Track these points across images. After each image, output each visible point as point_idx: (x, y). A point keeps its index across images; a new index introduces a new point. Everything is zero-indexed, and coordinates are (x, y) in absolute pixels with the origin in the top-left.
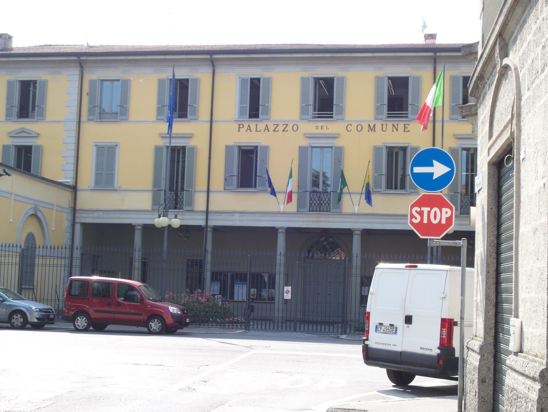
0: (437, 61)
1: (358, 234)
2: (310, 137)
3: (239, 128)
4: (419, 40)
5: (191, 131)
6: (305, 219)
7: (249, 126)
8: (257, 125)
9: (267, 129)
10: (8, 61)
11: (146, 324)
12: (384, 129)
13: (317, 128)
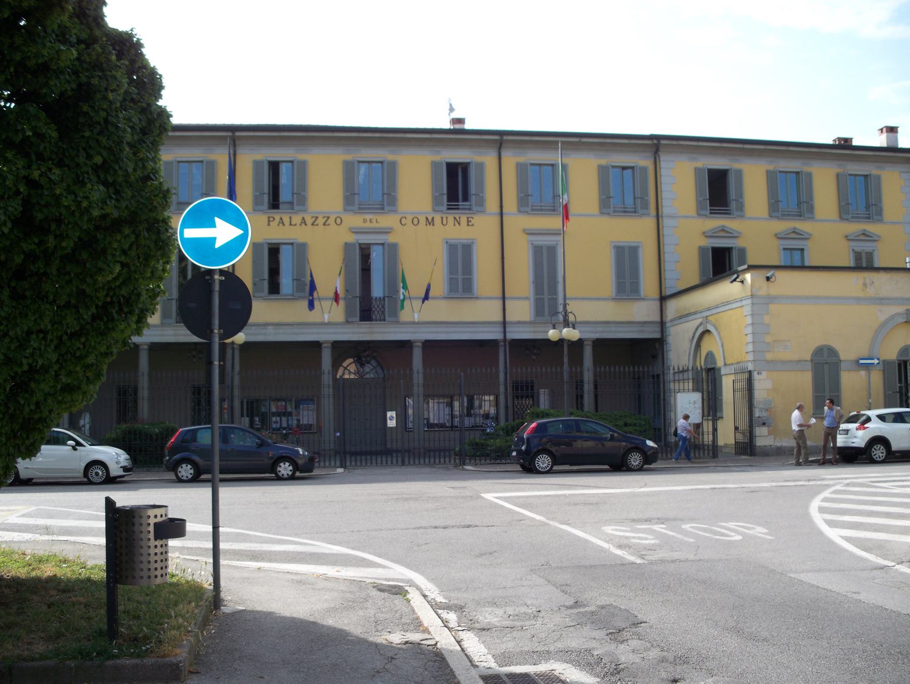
0: (237, 142)
2: (355, 231)
4: (445, 124)
5: (350, 227)
6: (356, 330)
9: (304, 222)
10: (698, 146)
11: (273, 468)
12: (444, 223)
13: (365, 221)
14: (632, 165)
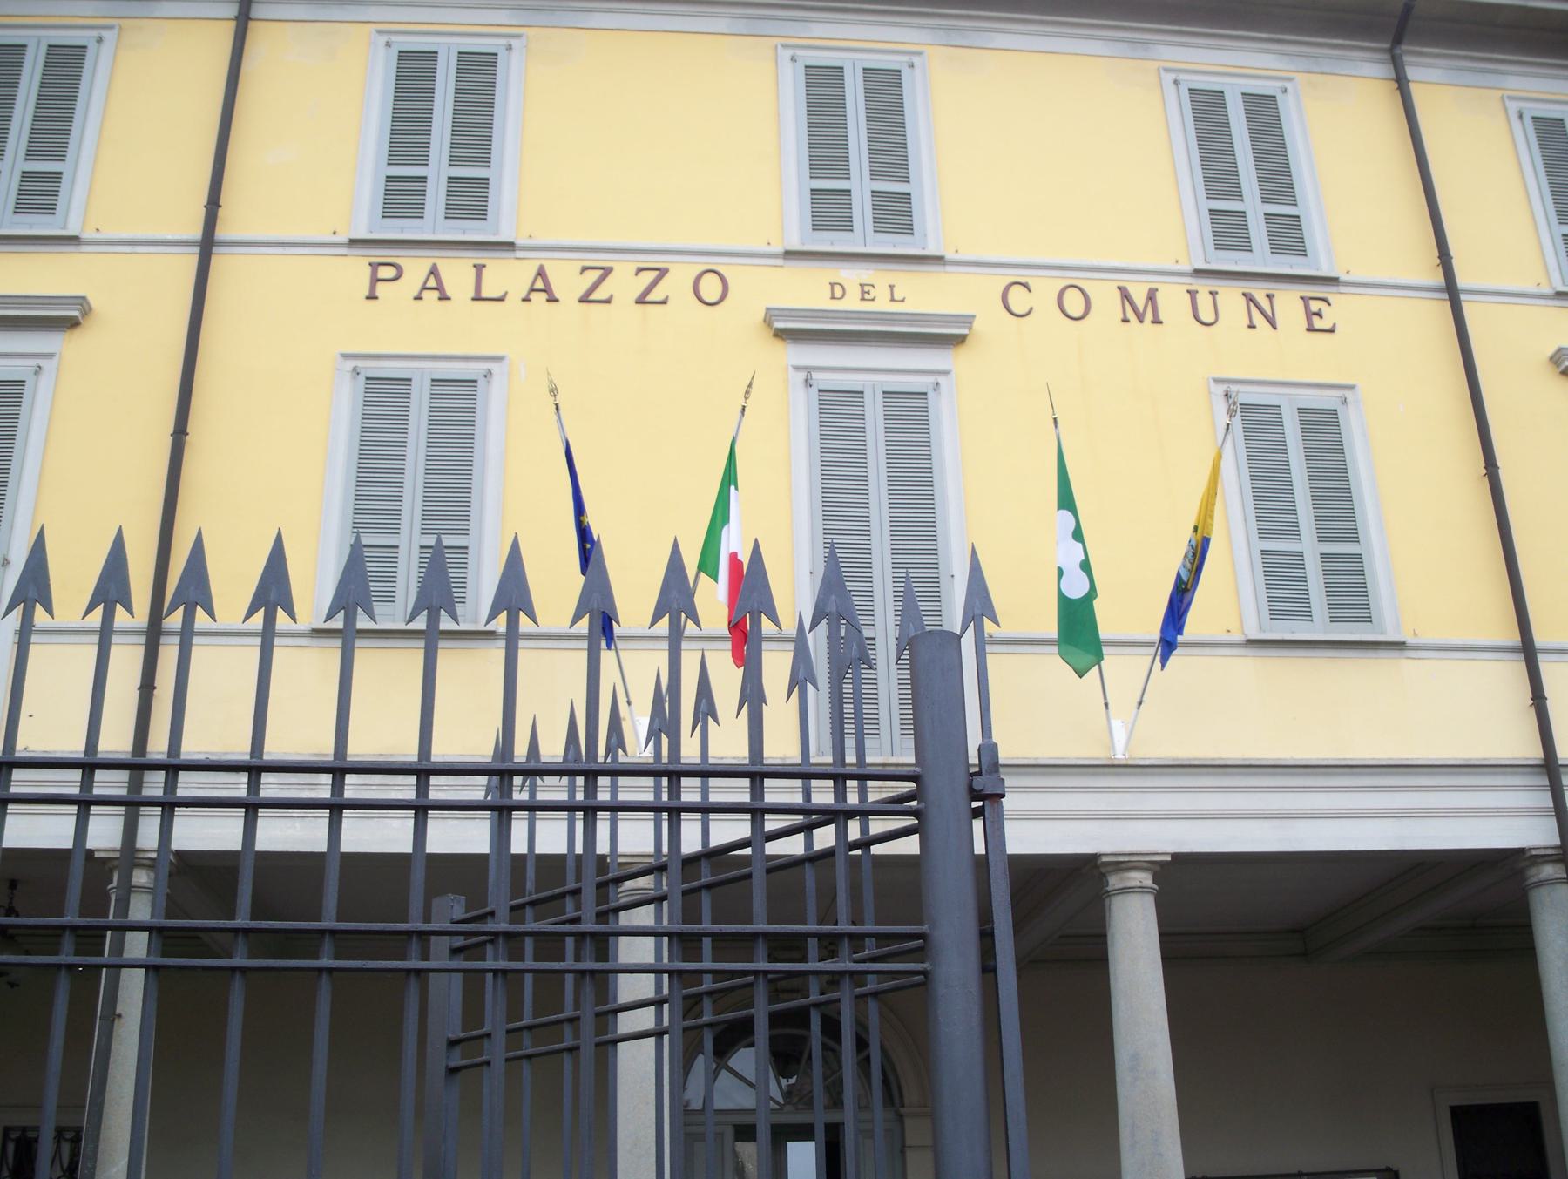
1: (1142, 890)
3: (375, 280)
7: (434, 272)
8: (479, 268)
9: (543, 286)
12: (1207, 316)
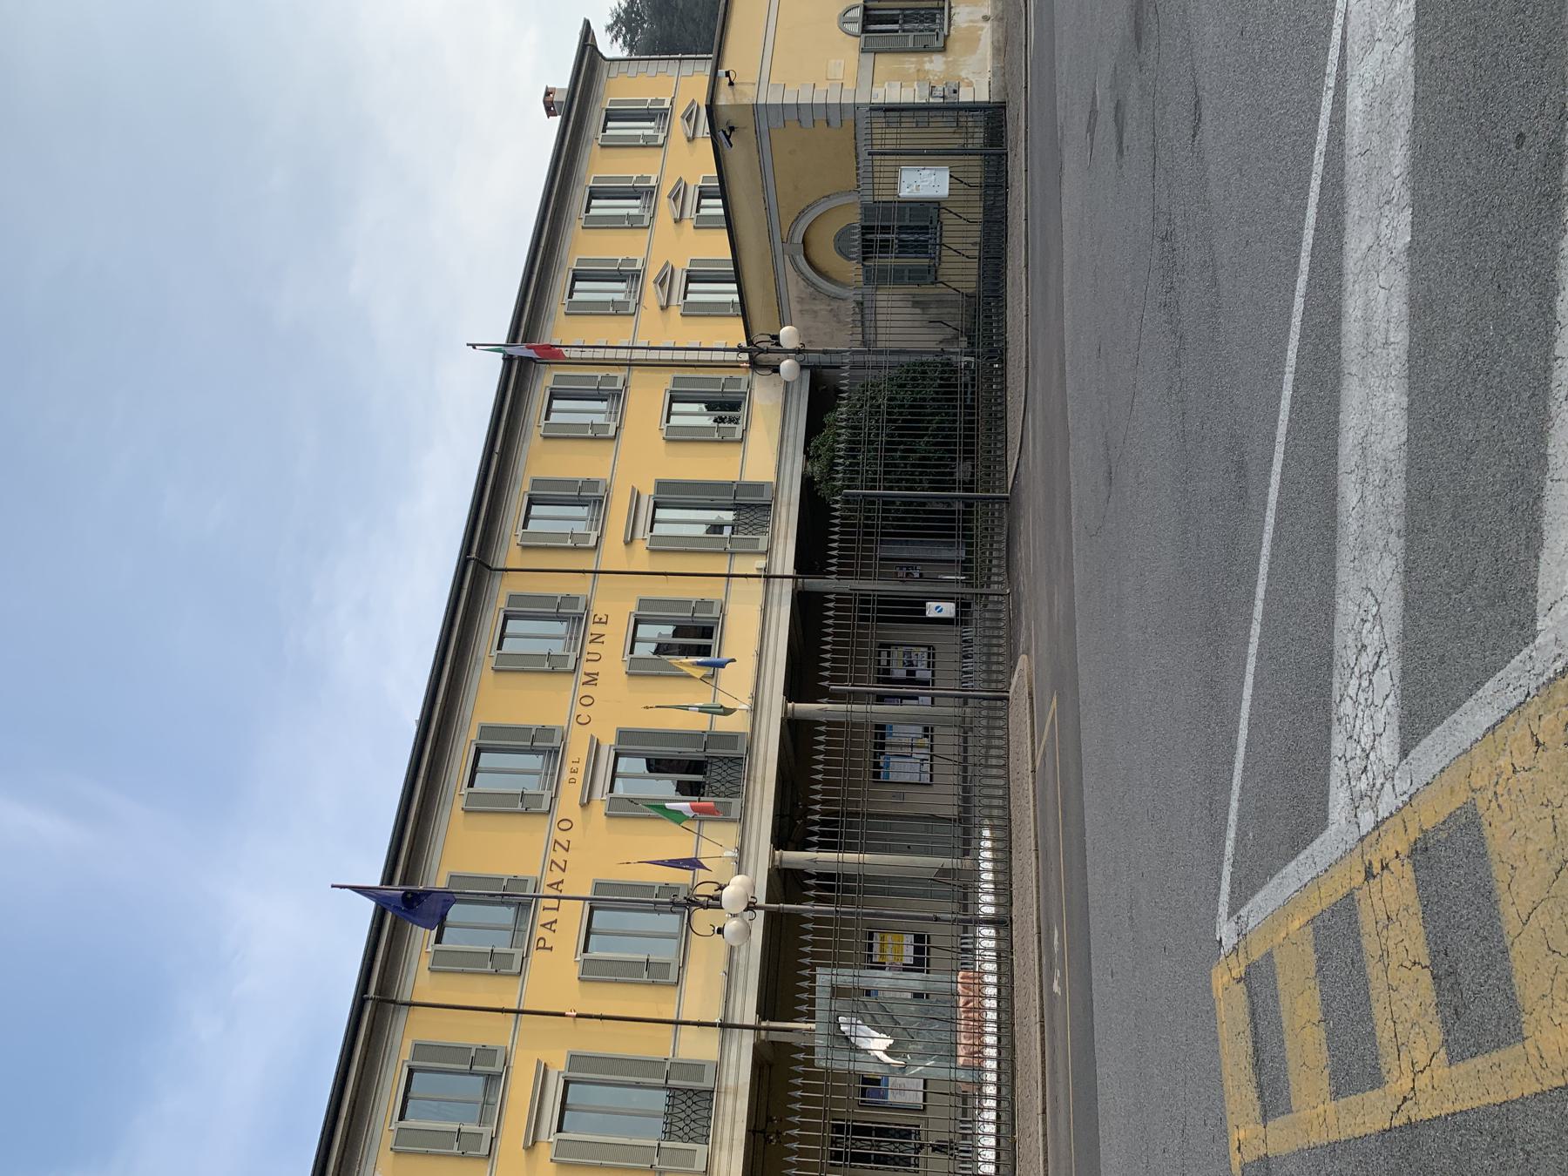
13: (572, 781)
14: (406, 1071)
